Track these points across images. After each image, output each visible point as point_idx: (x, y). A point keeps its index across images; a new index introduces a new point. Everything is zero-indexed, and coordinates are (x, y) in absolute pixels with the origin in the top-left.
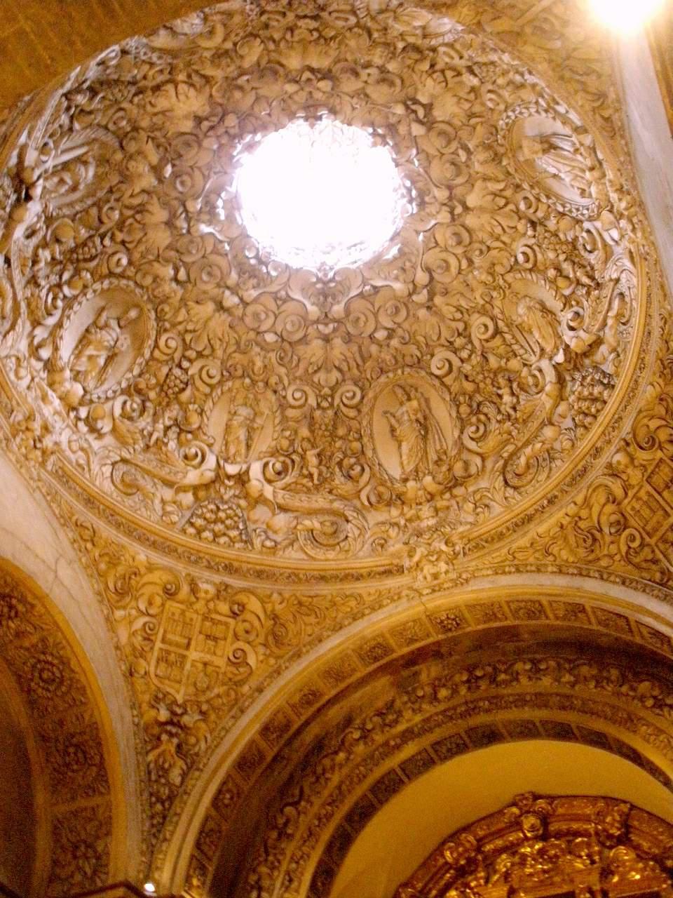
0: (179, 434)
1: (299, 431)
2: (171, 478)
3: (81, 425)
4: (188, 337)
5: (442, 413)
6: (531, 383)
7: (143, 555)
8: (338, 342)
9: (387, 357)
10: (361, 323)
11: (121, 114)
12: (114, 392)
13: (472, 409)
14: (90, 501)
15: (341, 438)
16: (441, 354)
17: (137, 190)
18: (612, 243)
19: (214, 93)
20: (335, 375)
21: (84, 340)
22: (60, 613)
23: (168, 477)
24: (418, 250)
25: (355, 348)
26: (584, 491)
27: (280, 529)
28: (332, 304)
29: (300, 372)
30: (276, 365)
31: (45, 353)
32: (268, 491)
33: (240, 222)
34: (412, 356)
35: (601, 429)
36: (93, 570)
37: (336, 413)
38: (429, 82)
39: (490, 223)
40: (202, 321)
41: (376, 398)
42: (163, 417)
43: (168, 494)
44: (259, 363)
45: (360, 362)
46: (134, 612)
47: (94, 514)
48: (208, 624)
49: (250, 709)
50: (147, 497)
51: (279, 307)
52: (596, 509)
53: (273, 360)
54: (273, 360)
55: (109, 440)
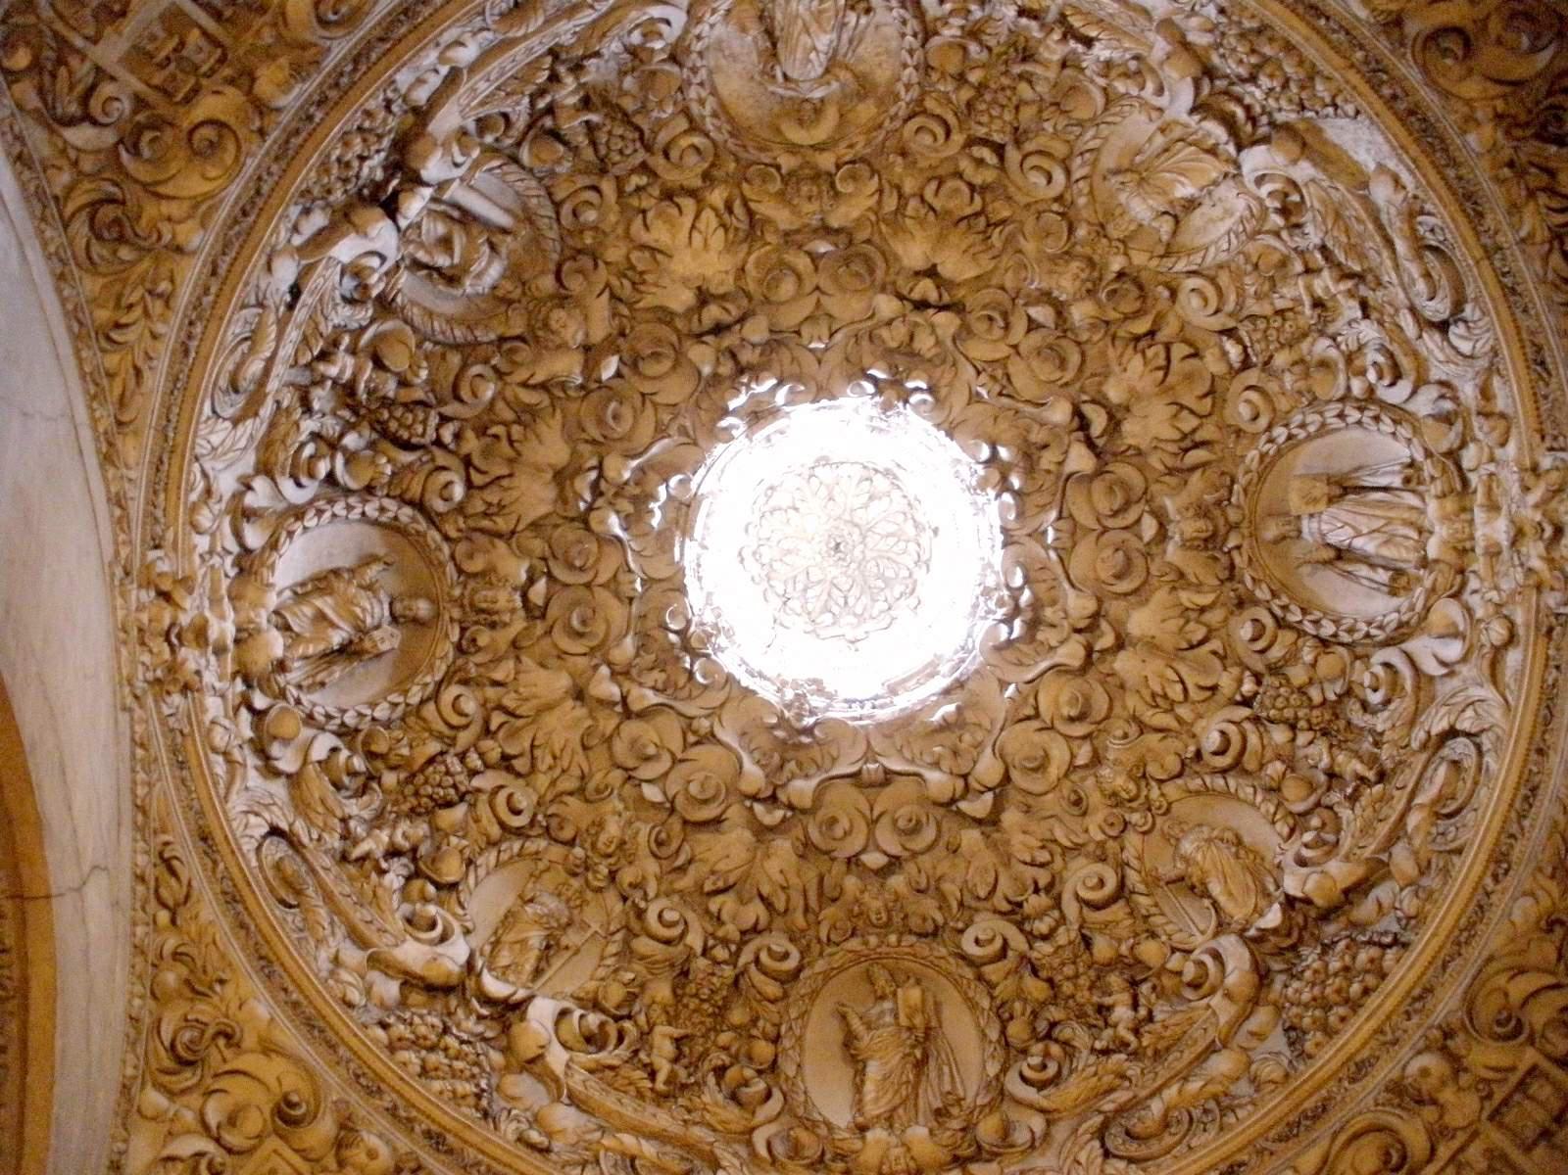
0: (408, 879)
1: (651, 985)
2: (370, 933)
4: (497, 719)
5: (966, 1037)
6: (1367, 683)
7: (261, 1009)
8: (783, 846)
9: (874, 905)
10: (839, 832)
11: (591, 196)
12: (329, 717)
13: (1033, 1034)
15: (734, 1028)
16: (986, 925)
17: (539, 378)
19: (749, 267)
20: (755, 912)
22: (52, 960)
23: (362, 927)
24: (992, 723)
25: (811, 876)
26: (1324, 1143)
27: (563, 1131)
28: (793, 777)
30: (643, 851)
32: (557, 1058)
33: (677, 557)
34: (924, 919)
35: (1373, 1024)
36: (147, 961)
37: (736, 982)
38: (1137, 362)
39: (1162, 676)
40: (535, 702)
41: (827, 976)
42: (394, 828)
43: (353, 956)
44: (613, 829)
45: (813, 903)
46: (189, 1117)
47: (204, 865)
50: (312, 930)
51: (686, 746)
53: (642, 838)
54: (642, 838)
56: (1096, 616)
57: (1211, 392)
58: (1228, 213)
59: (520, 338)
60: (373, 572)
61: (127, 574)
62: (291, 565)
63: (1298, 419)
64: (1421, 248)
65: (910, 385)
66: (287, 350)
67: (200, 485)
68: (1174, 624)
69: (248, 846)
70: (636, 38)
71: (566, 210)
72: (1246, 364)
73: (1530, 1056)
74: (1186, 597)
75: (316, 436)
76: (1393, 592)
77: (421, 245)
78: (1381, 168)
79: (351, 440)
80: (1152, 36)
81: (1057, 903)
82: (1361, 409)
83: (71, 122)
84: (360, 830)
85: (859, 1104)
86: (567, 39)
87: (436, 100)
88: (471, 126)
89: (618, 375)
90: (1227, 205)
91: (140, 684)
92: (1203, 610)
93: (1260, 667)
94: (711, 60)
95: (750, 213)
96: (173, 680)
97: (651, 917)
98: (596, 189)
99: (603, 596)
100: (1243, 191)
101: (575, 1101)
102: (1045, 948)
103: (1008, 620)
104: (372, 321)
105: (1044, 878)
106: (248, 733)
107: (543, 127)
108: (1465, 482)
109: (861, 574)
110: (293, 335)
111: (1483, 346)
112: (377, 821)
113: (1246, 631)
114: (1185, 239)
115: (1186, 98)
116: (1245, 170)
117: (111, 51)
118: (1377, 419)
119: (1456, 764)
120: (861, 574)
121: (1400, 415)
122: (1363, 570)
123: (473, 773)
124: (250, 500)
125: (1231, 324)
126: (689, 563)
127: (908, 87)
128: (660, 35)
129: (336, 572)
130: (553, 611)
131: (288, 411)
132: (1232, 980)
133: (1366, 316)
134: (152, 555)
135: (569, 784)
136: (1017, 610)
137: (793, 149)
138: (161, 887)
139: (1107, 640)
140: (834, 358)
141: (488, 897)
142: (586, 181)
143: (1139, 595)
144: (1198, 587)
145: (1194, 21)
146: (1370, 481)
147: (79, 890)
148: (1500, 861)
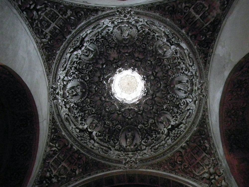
3: (64, 102)
11: (103, 48)
12: (73, 102)
14: (59, 115)
18: (189, 102)
19: (119, 56)
20: (117, 122)
21: (73, 88)
29: (110, 119)
31: (65, 83)
32: (95, 138)
43: (74, 127)
45: (123, 122)
48: (71, 158)
49: (71, 185)
51: (111, 105)
52: (176, 157)
55: (67, 109)
56: (153, 94)
57: (167, 71)
58: (170, 52)
59: (95, 63)
60: (78, 87)
61: (50, 87)
62: (69, 86)
63: (176, 75)
64: (190, 57)
65: (135, 69)
66: (69, 63)
67: (59, 77)
68: (161, 95)
69: (63, 116)
70: (107, 31)
71: (100, 49)
72: (170, 68)
73: (196, 145)
74: (163, 92)
75: (72, 72)
76: (185, 93)
77: (84, 52)
78: (186, 49)
79: (76, 73)
80: (162, 33)
81: (148, 123)
82: (182, 74)
83: (43, 38)
84: (76, 113)
85: (126, 144)
86: (100, 31)
87: (85, 37)
88: (89, 40)
89: (105, 67)
90: (170, 51)
91: (51, 99)
92: (164, 94)
93: (170, 100)
94: (115, 33)
95: (119, 50)
96: (55, 98)
97: (106, 123)
98: (103, 47)
99: (104, 90)
100: (171, 50)
101: (98, 143)
102: (146, 128)
103: (144, 94)
104: (79, 60)
105: (147, 120)
106: (64, 104)
107: (97, 40)
108: (193, 83)
109: (130, 88)
110: (69, 62)
111: (196, 68)
112: (78, 113)
113: (169, 96)
114: (165, 55)
115: (166, 40)
116: (172, 48)
117: (47, 31)
118: (184, 75)
119: (190, 113)
120: (130, 88)
121: (187, 75)
122: (182, 91)
123: (89, 108)
124: (65, 79)
125: (169, 64)
126: (112, 86)
127: (136, 37)
128: (110, 31)
129: (74, 87)
130: (98, 91)
131: (69, 70)
132: (165, 133)
133: (184, 64)
134: (53, 85)
135: (99, 109)
136: (145, 93)
137: (124, 44)
138: (53, 121)
139: (154, 96)
140: (128, 66)
141: (89, 120)
142: (102, 46)
143: (158, 92)
144: (164, 91)
145: (167, 32)
146: (183, 82)
147: (43, 122)
148: (193, 123)
